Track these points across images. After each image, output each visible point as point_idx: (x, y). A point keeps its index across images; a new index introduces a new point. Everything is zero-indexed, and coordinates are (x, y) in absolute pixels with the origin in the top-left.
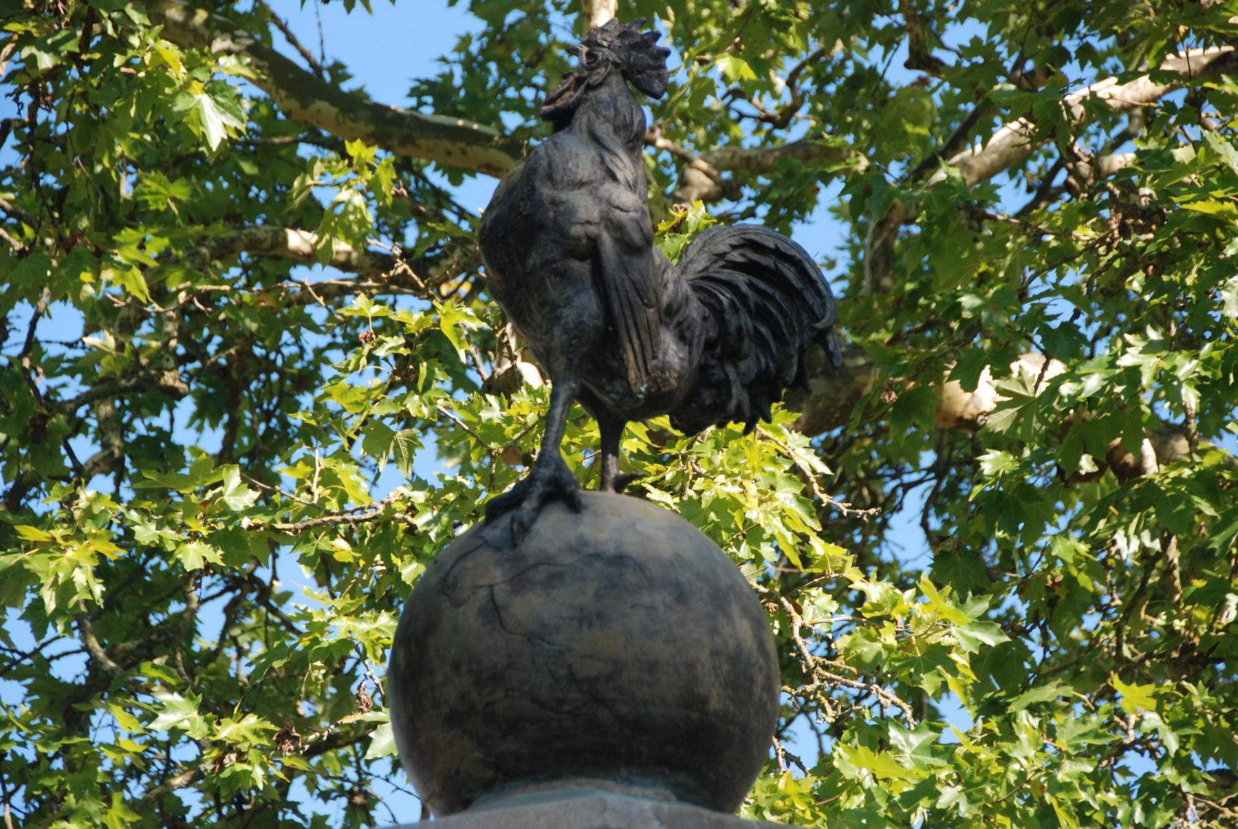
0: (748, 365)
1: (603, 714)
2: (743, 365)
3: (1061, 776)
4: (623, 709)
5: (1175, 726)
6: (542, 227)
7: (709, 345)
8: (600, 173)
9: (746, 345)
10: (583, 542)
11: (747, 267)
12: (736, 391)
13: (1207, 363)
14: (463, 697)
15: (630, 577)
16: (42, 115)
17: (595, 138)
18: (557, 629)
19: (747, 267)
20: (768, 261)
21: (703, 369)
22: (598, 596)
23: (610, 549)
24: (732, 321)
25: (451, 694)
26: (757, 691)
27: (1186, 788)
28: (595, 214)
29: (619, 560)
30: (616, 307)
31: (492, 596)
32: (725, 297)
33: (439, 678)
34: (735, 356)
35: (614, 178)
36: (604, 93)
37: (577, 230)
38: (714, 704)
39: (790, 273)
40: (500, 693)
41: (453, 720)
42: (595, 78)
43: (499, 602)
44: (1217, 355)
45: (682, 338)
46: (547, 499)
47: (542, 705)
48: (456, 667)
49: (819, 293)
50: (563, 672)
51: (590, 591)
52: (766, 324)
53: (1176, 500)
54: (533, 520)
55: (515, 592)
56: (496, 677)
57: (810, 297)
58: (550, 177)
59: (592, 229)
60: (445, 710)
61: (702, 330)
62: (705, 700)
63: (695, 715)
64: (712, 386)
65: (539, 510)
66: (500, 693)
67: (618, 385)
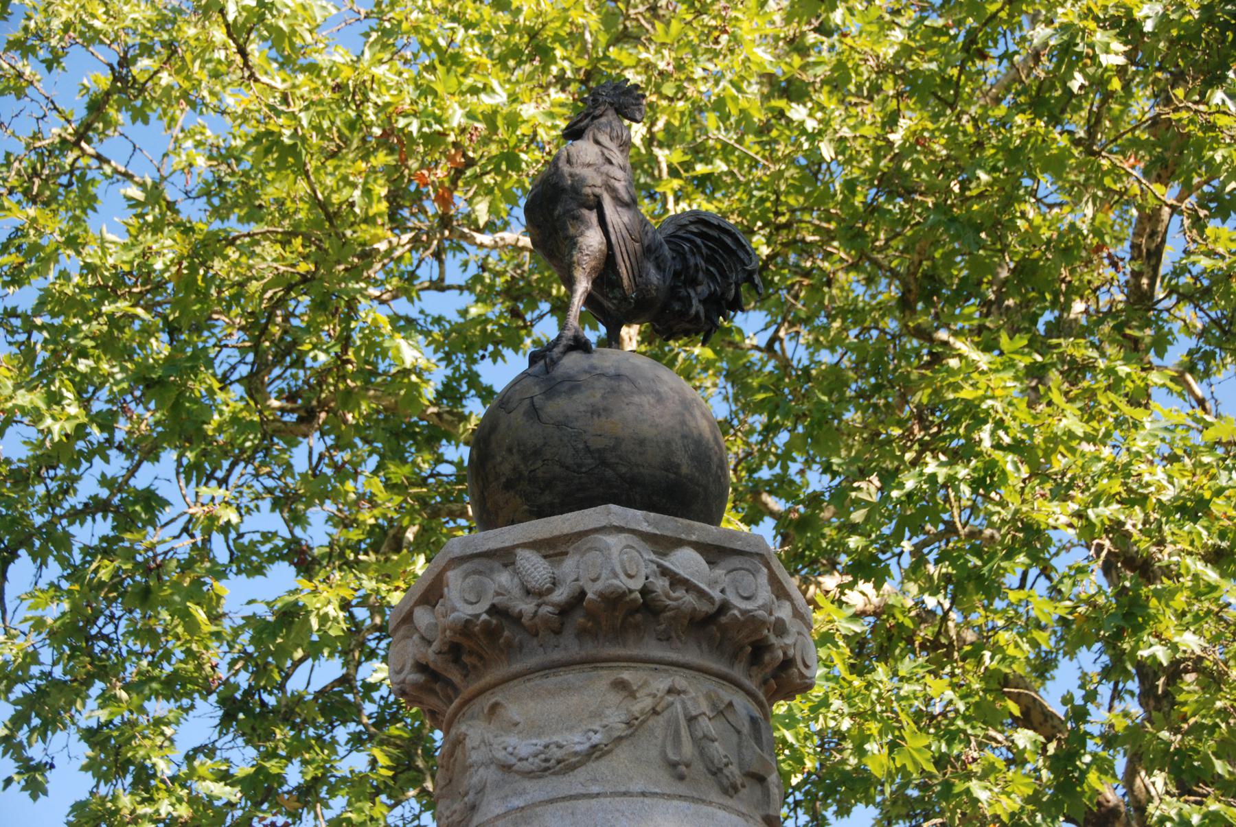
0: (703, 289)
1: (609, 473)
2: (699, 289)
3: (902, 693)
4: (623, 470)
5: (962, 697)
6: (564, 190)
7: (677, 274)
8: (601, 160)
9: (701, 276)
10: (593, 367)
11: (701, 235)
12: (695, 302)
13: (975, 470)
14: (514, 469)
15: (625, 386)
16: (272, 164)
17: (597, 142)
18: (577, 419)
19: (701, 235)
20: (714, 233)
21: (673, 289)
22: (603, 397)
23: (612, 371)
24: (692, 261)
25: (506, 468)
26: (714, 467)
27: (970, 731)
28: (599, 181)
29: (618, 376)
30: (613, 238)
31: (533, 404)
32: (686, 246)
33: (499, 459)
34: (694, 283)
35: (611, 163)
36: (603, 120)
37: (588, 190)
38: (685, 470)
39: (728, 241)
40: (539, 463)
41: (509, 486)
42: (598, 112)
43: (537, 405)
44: (980, 465)
45: (659, 268)
46: (570, 349)
47: (568, 468)
48: (510, 450)
49: (747, 253)
50: (581, 446)
51: (598, 395)
52: (713, 265)
53: (959, 557)
54: (560, 359)
55: (548, 399)
56: (537, 453)
57: (742, 255)
58: (569, 161)
59: (597, 191)
60: (503, 479)
61: (672, 265)
62: (678, 466)
63: (672, 476)
64: (680, 299)
65: (564, 353)
66: (539, 463)
67: (617, 293)
